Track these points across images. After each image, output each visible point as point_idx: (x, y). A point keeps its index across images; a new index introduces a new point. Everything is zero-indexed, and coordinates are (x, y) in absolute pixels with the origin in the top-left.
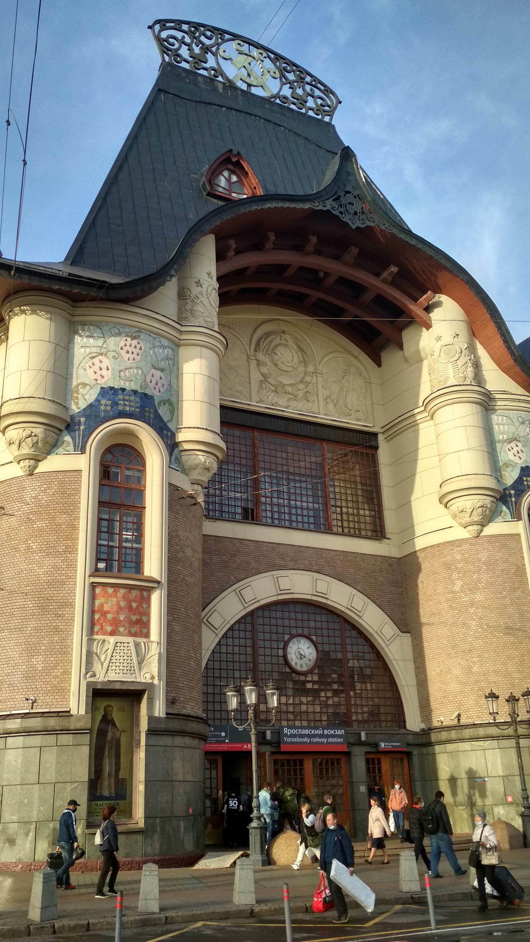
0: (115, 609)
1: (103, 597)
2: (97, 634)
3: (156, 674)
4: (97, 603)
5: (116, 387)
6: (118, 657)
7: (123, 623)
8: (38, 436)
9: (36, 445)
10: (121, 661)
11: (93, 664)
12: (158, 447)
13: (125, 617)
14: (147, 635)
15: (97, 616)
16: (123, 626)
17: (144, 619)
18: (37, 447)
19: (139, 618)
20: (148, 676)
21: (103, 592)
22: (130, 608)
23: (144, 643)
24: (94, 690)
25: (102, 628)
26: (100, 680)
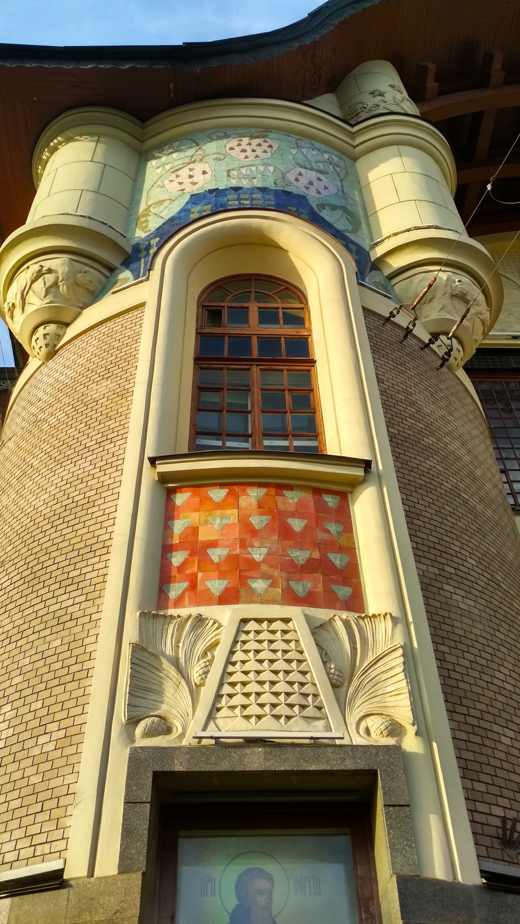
0: (236, 534)
1: (197, 510)
2: (178, 603)
3: (404, 713)
4: (179, 526)
5: (220, 188)
6: (252, 666)
7: (264, 568)
8: (56, 272)
9: (53, 290)
10: (267, 676)
11: (160, 693)
12: (322, 247)
13: (268, 554)
14: (355, 602)
15: (177, 559)
16: (265, 576)
17: (337, 560)
18: (57, 294)
19: (316, 555)
20: (375, 724)
21: (197, 499)
22: (286, 533)
23: (346, 624)
24: (161, 779)
25: (193, 586)
26: (184, 743)
